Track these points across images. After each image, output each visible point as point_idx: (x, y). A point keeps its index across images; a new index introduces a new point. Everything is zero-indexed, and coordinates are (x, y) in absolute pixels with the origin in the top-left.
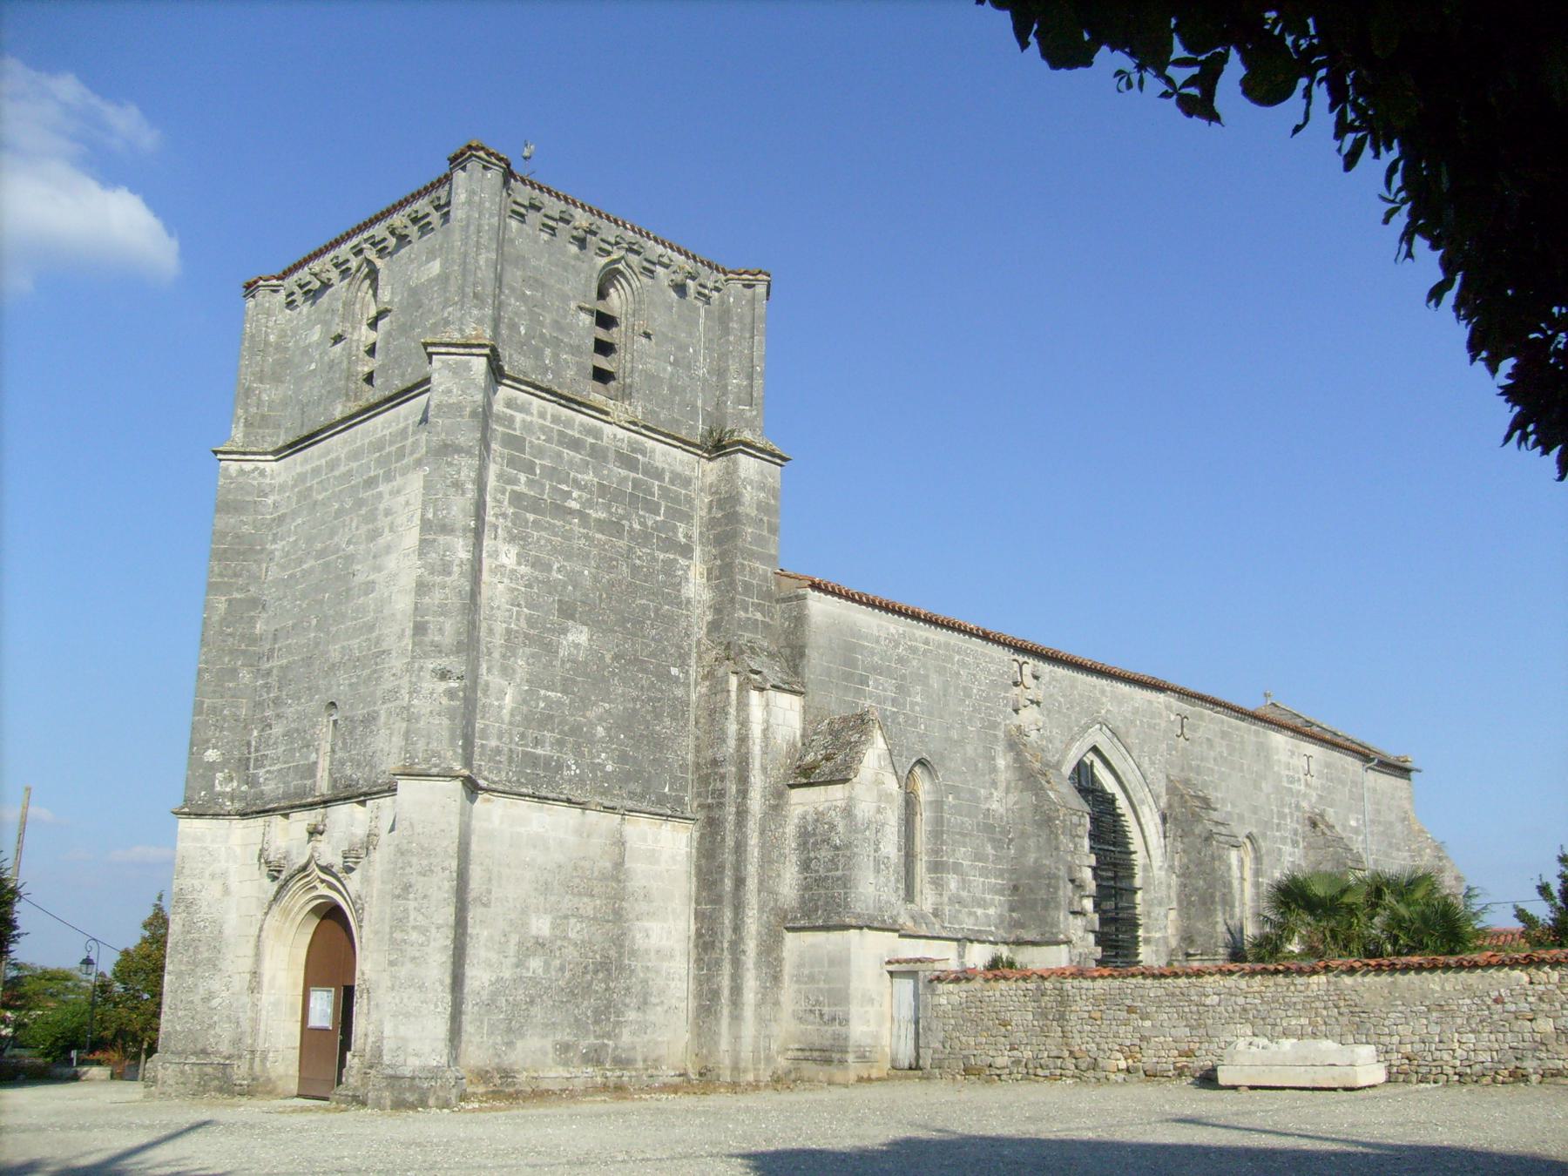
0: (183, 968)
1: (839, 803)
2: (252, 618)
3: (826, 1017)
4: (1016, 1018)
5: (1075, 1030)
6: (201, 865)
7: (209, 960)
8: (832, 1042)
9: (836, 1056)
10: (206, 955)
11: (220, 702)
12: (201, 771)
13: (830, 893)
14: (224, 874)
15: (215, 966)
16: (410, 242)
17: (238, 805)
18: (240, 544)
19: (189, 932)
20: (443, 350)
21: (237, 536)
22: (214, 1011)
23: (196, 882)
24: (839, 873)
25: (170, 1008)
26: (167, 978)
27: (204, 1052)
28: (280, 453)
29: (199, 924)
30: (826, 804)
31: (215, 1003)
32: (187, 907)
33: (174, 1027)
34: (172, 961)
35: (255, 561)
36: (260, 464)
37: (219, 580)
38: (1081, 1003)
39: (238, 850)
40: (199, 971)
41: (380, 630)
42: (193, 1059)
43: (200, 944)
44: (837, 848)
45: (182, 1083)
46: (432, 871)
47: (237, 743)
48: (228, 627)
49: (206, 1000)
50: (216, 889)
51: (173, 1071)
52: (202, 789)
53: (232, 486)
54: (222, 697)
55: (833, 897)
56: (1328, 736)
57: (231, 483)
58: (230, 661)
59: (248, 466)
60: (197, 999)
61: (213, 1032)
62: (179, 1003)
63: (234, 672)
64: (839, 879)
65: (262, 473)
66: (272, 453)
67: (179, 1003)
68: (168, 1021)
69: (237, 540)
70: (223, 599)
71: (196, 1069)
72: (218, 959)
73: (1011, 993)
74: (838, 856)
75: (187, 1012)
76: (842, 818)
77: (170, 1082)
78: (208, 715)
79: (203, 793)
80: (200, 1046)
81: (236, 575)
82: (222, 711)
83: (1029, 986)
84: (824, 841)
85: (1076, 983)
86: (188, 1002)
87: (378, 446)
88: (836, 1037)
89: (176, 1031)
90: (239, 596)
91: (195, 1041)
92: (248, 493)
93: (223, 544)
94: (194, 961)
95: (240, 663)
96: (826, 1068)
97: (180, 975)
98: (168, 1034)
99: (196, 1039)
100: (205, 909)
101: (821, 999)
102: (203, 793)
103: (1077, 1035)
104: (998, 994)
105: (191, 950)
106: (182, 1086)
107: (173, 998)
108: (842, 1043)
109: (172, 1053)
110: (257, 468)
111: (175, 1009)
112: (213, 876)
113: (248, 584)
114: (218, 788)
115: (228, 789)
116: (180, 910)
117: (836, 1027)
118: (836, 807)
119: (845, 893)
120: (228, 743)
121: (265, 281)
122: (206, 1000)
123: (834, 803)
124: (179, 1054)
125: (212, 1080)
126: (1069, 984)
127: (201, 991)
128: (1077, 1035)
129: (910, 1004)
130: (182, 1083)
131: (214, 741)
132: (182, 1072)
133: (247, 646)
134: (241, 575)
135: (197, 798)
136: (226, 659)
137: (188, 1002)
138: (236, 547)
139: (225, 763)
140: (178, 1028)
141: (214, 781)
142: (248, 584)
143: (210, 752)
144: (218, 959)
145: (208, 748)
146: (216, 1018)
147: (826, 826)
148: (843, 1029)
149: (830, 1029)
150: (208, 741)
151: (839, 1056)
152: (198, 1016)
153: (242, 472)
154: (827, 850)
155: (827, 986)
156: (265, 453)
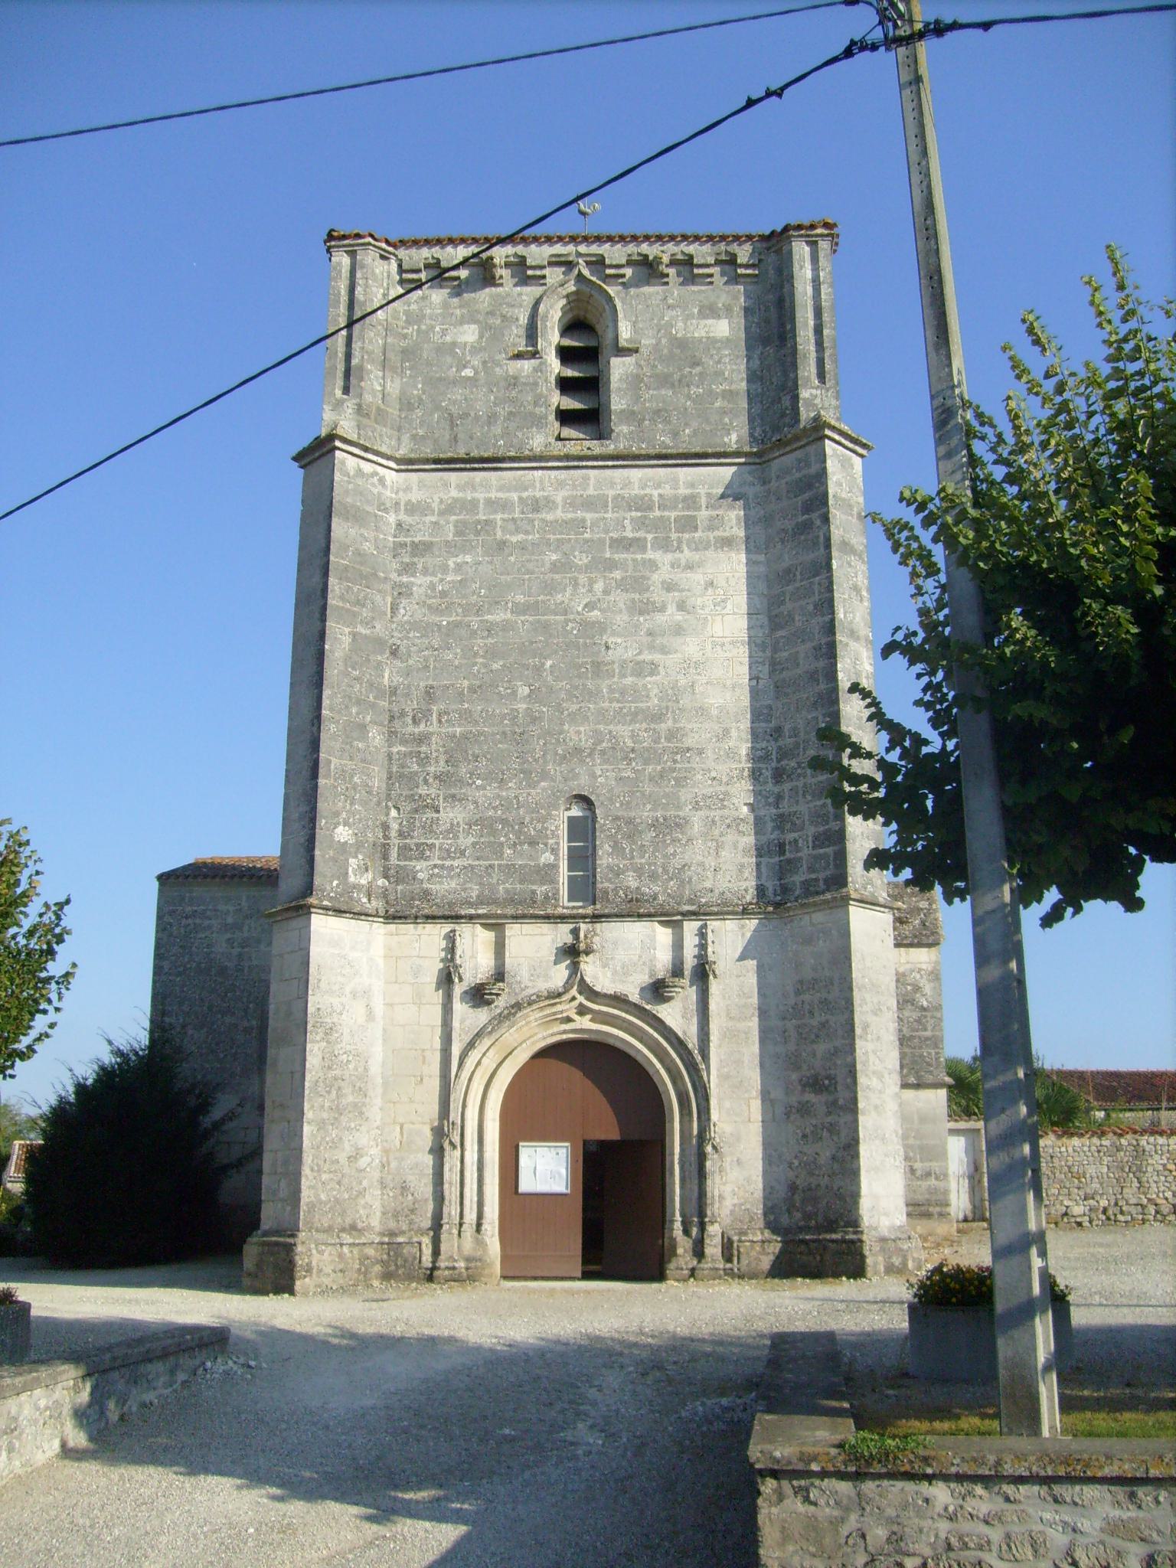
0: (325, 1115)
1: (924, 967)
2: (379, 663)
3: (919, 1173)
4: (1091, 1170)
5: (1151, 1180)
6: (340, 979)
7: (355, 1105)
8: (927, 1196)
9: (935, 1210)
10: (350, 1099)
11: (350, 765)
12: (331, 853)
13: (917, 1052)
14: (367, 993)
15: (361, 1113)
16: (667, 283)
17: (377, 904)
18: (362, 564)
19: (330, 1068)
20: (837, 437)
21: (358, 553)
22: (363, 1174)
23: (335, 1001)
24: (928, 1033)
25: (312, 1170)
26: (307, 1129)
27: (353, 1228)
28: (407, 464)
29: (341, 1058)
30: (908, 966)
31: (363, 1162)
32: (326, 1034)
33: (317, 1196)
34: (313, 1106)
35: (379, 591)
36: (379, 469)
37: (341, 604)
38: (1157, 1157)
39: (381, 962)
40: (344, 1119)
41: (675, 721)
42: (347, 1239)
43: (342, 1084)
44: (923, 1009)
45: (341, 1271)
46: (880, 1010)
47: (370, 823)
48: (354, 669)
49: (353, 1159)
50: (358, 1011)
51: (330, 1254)
52: (333, 877)
53: (351, 486)
54: (351, 759)
55: (921, 1056)
56: (363, 917)
57: (350, 483)
58: (358, 714)
59: (367, 467)
60: (342, 1157)
61: (362, 1202)
62: (321, 1163)
63: (363, 728)
64: (927, 1039)
65: (382, 481)
66: (398, 461)
67: (321, 1163)
68: (310, 1187)
69: (358, 559)
70: (347, 630)
71: (356, 1251)
72: (364, 1104)
73: (1086, 1149)
74: (926, 1017)
75: (331, 1175)
76: (929, 981)
77: (328, 1270)
78: (335, 780)
79: (335, 883)
80: (348, 1221)
81: (358, 603)
82: (352, 777)
83: (1104, 1143)
84: (908, 1001)
85: (1152, 1139)
86: (333, 1162)
87: (642, 504)
88: (933, 1191)
89: (321, 1202)
90: (364, 631)
91: (343, 1213)
92: (368, 502)
93: (343, 558)
94: (338, 1106)
95: (368, 718)
96: (925, 1222)
97: (322, 1125)
98: (312, 1206)
99: (344, 1211)
100: (346, 1038)
101: (911, 1154)
102: (335, 883)
103: (1154, 1185)
104: (1070, 1150)
105: (334, 1092)
106: (339, 1274)
107: (315, 1157)
108: (941, 1197)
109: (317, 1231)
110: (375, 474)
111: (319, 1171)
112: (354, 995)
113: (373, 618)
114: (352, 879)
115: (363, 882)
116: (318, 1038)
117: (932, 1182)
118: (920, 970)
119: (937, 1053)
120: (360, 820)
121: (375, 239)
122: (353, 1159)
123: (919, 966)
124: (328, 1230)
125: (373, 1264)
126: (1144, 1141)
127: (347, 1146)
128: (1154, 1185)
129: (961, 1161)
130: (341, 1271)
131: (344, 815)
132: (341, 1256)
133: (375, 698)
134: (363, 606)
135: (328, 888)
136: (354, 710)
137: (333, 1162)
138: (358, 567)
139: (359, 846)
140: (323, 1197)
141: (347, 869)
142: (373, 618)
143: (340, 829)
144: (364, 1104)
145: (339, 824)
146: (365, 1183)
147: (909, 988)
148: (941, 1184)
149: (925, 1184)
150: (337, 814)
151: (938, 1209)
152: (346, 1181)
153: (360, 472)
154: (911, 1011)
155: (918, 1142)
156: (389, 458)
